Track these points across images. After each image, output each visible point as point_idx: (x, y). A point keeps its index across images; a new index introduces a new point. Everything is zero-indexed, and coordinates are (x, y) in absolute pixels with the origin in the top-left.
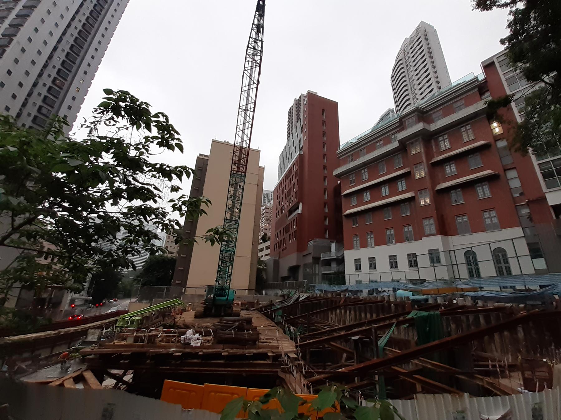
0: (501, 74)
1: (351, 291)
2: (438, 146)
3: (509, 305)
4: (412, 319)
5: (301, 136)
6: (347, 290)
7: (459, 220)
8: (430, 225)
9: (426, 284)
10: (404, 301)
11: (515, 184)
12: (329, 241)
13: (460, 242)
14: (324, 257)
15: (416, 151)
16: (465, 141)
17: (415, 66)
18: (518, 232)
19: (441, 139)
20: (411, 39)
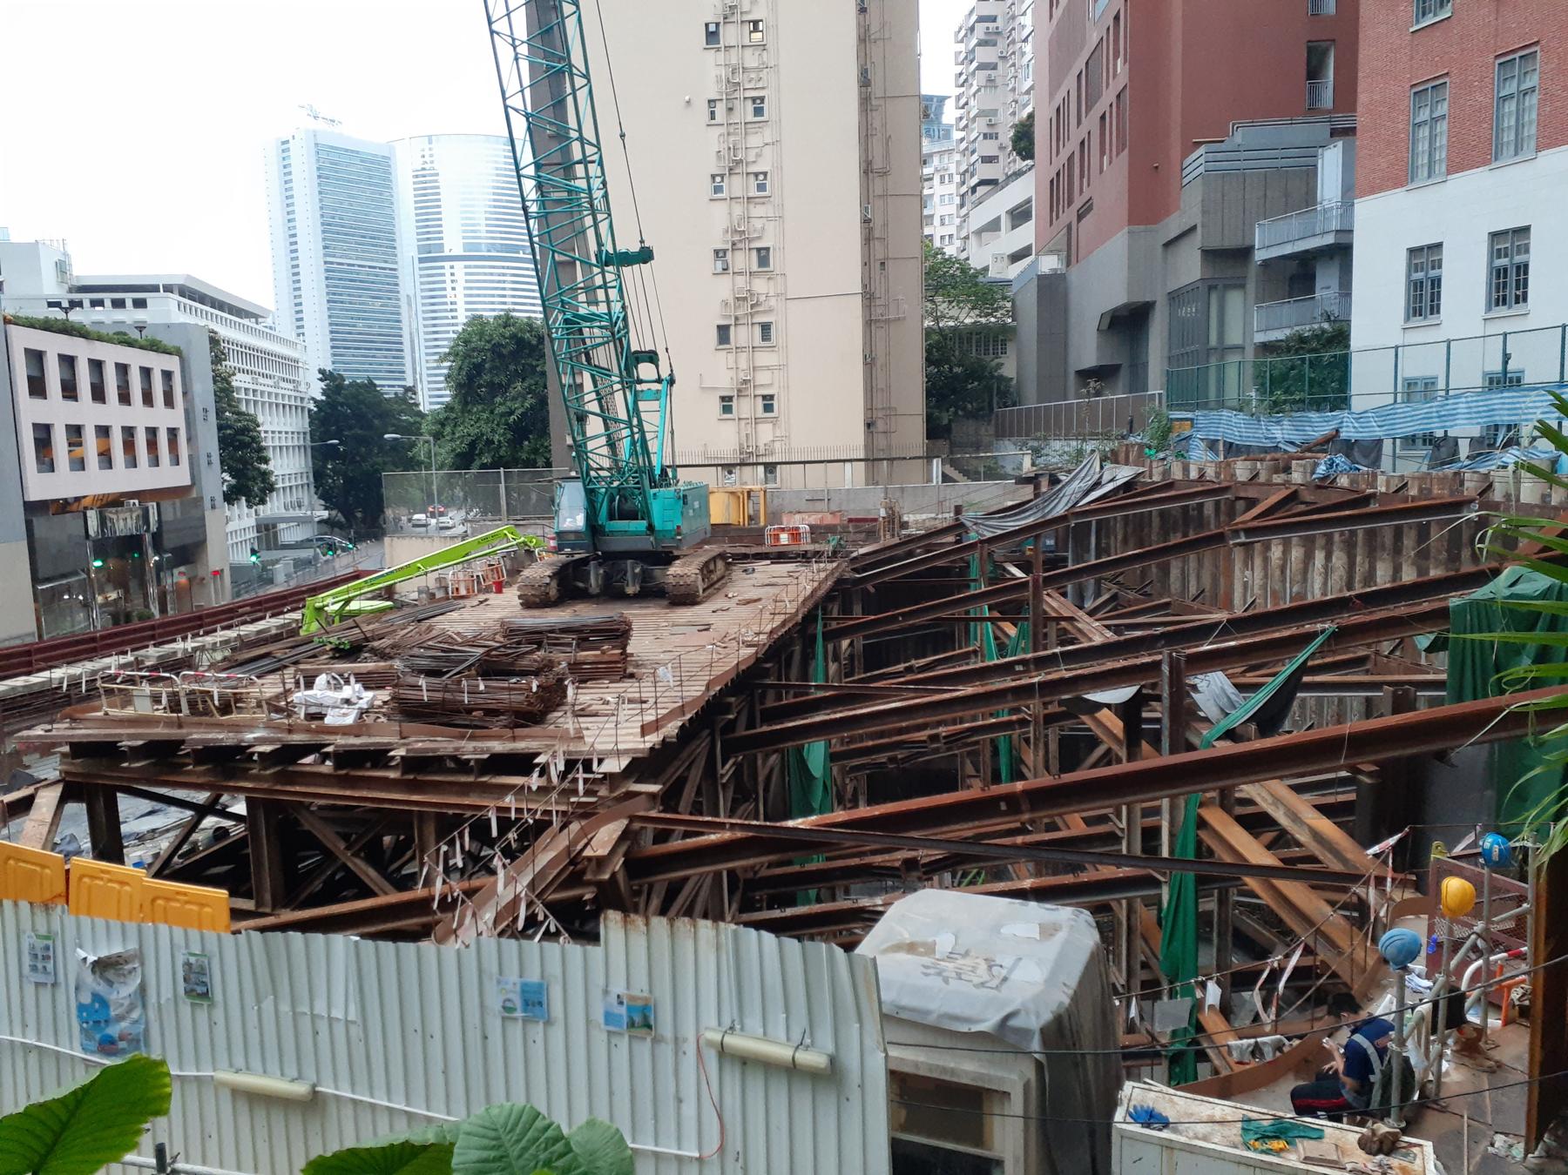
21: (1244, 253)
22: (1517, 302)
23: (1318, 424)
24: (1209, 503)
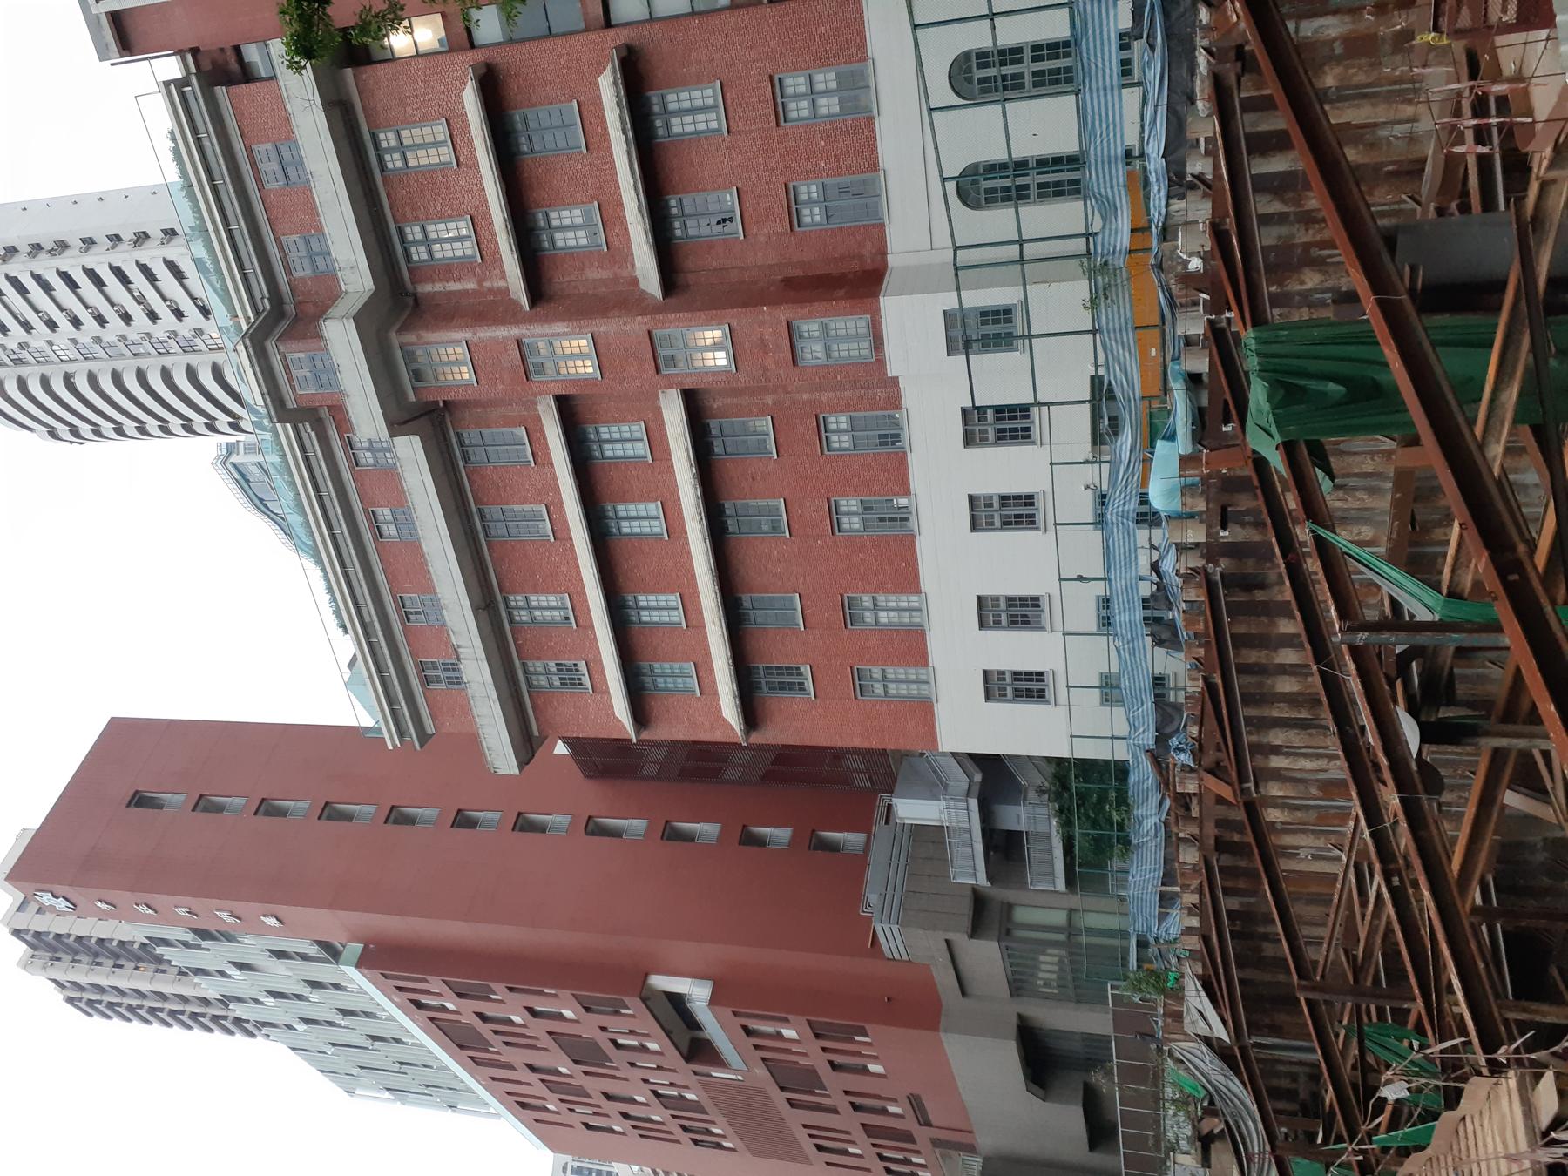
1: (1162, 739)
2: (449, 269)
3: (1202, 60)
5: (251, 947)
6: (1158, 757)
7: (812, 216)
8: (827, 335)
9: (1116, 377)
10: (1205, 480)
12: (880, 829)
13: (916, 219)
14: (969, 868)
15: (459, 363)
16: (446, 154)
19: (419, 254)
21: (979, 901)
22: (1032, 504)
23: (1143, 775)
24: (1228, 903)
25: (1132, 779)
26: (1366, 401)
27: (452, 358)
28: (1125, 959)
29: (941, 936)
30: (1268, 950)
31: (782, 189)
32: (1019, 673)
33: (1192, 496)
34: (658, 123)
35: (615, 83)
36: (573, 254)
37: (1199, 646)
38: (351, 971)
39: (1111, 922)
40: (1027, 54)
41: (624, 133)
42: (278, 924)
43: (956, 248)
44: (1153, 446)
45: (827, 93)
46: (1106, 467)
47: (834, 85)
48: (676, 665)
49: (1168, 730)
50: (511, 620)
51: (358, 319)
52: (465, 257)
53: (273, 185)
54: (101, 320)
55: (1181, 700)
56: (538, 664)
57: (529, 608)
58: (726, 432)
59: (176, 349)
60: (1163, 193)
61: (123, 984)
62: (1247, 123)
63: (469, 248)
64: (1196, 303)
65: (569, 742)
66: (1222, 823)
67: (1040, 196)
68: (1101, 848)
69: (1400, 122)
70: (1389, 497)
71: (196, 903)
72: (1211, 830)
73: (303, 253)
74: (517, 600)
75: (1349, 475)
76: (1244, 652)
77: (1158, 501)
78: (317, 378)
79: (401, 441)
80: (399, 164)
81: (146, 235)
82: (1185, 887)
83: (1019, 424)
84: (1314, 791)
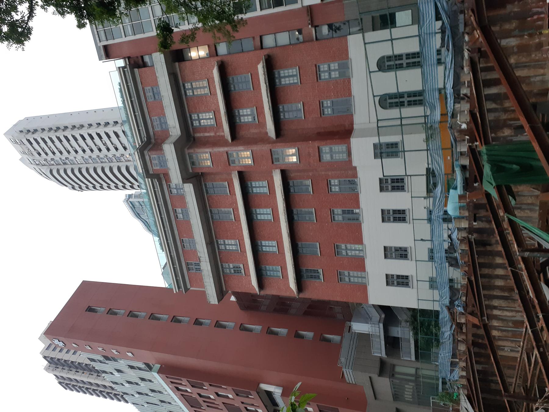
0: (124, 39)
1: (452, 302)
2: (205, 129)
3: (466, 54)
4: (499, 188)
5: (122, 364)
6: (450, 308)
7: (328, 111)
8: (331, 152)
9: (435, 167)
10: (468, 204)
11: (283, 38)
12: (346, 334)
13: (364, 111)
14: (379, 350)
15: (207, 159)
16: (207, 91)
17: (69, 152)
18: (355, 42)
19: (196, 123)
20: (24, 153)
21: (382, 363)
22: (406, 251)
23: (445, 315)
24: (476, 367)
25: (441, 317)
26: (529, 172)
27: (205, 158)
28: (437, 388)
29: (368, 375)
30: (493, 386)
31: (314, 66)
32: (399, 276)
33: (463, 210)
34: (277, 81)
35: (263, 67)
36: (247, 124)
37: (466, 266)
38: (156, 375)
39: (432, 373)
40: (404, 57)
41: (266, 83)
42: (132, 356)
43: (378, 120)
44: (449, 192)
45: (335, 70)
46: (431, 199)
47: (337, 68)
48: (274, 267)
49: (454, 299)
50: (219, 248)
51: (175, 144)
52: (211, 125)
53: (150, 100)
54: (92, 150)
55: (459, 287)
56: (227, 265)
57: (225, 244)
58: (295, 185)
59: (115, 160)
60: (452, 101)
61: (79, 378)
62: (483, 76)
63: (213, 122)
64: (464, 140)
65: (236, 294)
66: (474, 335)
67: (408, 105)
68: (428, 345)
69: (539, 76)
70: (538, 213)
71: (105, 346)
72: (470, 338)
73: (158, 123)
74: (221, 241)
75: (522, 204)
76: (483, 269)
77: (450, 212)
78: (160, 163)
79: (186, 185)
80: (191, 94)
81: (108, 123)
82: (460, 359)
83: (400, 184)
84: (511, 324)
